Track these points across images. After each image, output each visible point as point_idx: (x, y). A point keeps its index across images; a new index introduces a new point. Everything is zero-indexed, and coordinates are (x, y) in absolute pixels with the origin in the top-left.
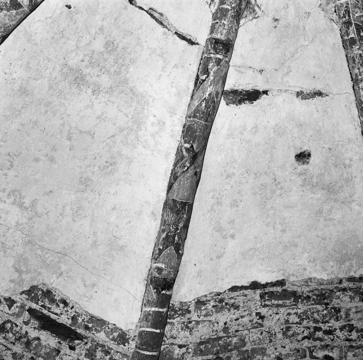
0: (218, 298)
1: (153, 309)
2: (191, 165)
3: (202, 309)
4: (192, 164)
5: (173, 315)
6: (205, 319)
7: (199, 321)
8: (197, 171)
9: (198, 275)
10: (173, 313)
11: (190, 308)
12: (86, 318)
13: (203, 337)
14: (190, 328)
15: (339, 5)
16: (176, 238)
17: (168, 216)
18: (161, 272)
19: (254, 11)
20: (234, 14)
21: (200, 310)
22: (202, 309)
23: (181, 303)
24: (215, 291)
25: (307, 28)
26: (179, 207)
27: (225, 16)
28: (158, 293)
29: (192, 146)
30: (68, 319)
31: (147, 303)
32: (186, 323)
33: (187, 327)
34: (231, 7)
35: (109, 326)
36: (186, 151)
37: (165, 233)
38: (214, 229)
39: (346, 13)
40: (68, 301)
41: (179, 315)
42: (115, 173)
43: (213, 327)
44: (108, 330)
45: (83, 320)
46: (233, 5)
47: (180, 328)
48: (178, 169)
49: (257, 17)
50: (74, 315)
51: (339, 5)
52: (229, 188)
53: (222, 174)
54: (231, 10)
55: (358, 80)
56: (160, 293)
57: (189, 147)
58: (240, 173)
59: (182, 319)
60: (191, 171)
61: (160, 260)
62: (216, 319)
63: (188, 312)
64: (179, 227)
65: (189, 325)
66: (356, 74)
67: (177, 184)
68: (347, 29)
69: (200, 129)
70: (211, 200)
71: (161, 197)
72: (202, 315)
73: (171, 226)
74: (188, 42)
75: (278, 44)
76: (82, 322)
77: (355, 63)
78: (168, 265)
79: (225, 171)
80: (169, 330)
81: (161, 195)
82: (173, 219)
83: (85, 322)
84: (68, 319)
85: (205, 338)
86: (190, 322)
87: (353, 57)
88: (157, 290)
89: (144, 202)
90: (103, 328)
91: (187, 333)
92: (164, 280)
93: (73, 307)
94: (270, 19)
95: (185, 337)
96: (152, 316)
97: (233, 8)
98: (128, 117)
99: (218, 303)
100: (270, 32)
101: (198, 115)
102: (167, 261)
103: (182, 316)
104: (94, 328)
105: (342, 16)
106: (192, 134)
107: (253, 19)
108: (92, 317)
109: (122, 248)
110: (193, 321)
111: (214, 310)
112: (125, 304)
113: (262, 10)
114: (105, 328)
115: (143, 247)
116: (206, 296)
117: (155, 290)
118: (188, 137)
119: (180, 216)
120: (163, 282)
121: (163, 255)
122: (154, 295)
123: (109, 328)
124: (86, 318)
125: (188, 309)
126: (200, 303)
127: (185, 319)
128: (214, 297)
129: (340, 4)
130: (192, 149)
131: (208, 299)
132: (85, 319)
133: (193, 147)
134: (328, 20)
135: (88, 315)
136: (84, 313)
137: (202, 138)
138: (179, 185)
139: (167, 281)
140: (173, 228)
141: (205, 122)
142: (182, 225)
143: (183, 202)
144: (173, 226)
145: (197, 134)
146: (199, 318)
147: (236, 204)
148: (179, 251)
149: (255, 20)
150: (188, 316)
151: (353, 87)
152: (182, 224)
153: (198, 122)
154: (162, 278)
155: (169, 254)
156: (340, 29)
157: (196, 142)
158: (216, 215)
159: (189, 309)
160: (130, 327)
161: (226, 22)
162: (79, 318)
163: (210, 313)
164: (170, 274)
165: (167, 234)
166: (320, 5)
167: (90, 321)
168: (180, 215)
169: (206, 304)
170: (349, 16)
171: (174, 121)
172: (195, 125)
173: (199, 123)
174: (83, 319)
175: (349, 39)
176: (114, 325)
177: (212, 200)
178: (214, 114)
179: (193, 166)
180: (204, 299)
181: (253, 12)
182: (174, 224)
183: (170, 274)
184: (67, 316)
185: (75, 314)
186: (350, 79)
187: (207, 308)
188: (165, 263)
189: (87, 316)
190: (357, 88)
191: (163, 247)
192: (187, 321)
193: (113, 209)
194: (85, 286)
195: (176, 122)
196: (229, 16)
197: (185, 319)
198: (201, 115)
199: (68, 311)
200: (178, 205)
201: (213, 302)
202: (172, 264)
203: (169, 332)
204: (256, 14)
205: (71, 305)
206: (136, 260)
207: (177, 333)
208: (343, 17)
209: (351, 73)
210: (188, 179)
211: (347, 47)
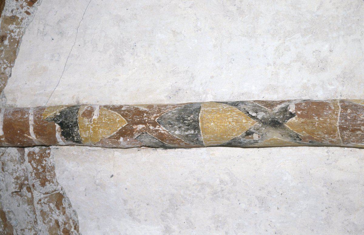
0: (71, 227)
1: (31, 118)
2: (261, 121)
3: (51, 204)
4: (263, 123)
5: (34, 159)
6: (38, 213)
7: (33, 204)
8: (254, 135)
9: (97, 185)
10: (38, 158)
11: (49, 183)
12: (16, 34)
13: (11, 216)
14: (20, 191)
16: (140, 127)
17: (173, 108)
18: (86, 116)
21: (49, 202)
22: (51, 204)
23: (53, 168)
24: (80, 218)
26: (189, 118)
28: (56, 119)
29: (292, 115)
30: (12, 11)
31: (40, 110)
32: (26, 182)
33: (21, 186)
35: (8, 69)
36: (282, 108)
37: (146, 109)
38: (173, 195)
40: (35, 4)
41: (36, 169)
42: (228, 18)
43: (29, 229)
44: (2, 68)
45: (13, 30)
47: (17, 174)
48: (250, 104)
50: (18, 18)
52: (243, 206)
53: (263, 188)
56: (56, 121)
57: (290, 110)
58: (273, 221)
59: (31, 175)
60: (250, 124)
61: (105, 110)
62: (40, 231)
63: (43, 181)
64: (158, 126)
65: (25, 189)
67: (225, 107)
69: (325, 122)
70: (218, 180)
71: (204, 95)
72: (42, 207)
73: (158, 115)
76: (9, 30)
78: (97, 123)
79: (269, 192)
80: (12, 157)
81: (208, 96)
82: (169, 114)
83: (9, 34)
84: (12, 11)
85: (10, 219)
86: (29, 189)
88: (59, 116)
89: (192, 74)
90: (5, 60)
91: (13, 188)
92: (75, 123)
93: (28, 13)
95: (6, 185)
96: (21, 118)
98: (318, 9)
99: (63, 228)
101: (349, 111)
102: (104, 121)
103: (35, 174)
104: (3, 48)
106: (313, 110)
108: (18, 42)
109: (119, 60)
110: (32, 193)
111: (51, 224)
112: (40, 83)
114: (4, 63)
115: (126, 90)
116: (70, 206)
117: (59, 114)
118: (307, 106)
119: (175, 125)
120: (72, 121)
121: (112, 113)
122: (51, 114)
123: (5, 68)
124: (16, 34)
125: (47, 181)
126: (59, 199)
127: (33, 180)
128: (71, 221)
130: (288, 115)
131: (68, 211)
132: (14, 33)
133: (291, 117)
135: (20, 36)
136: (22, 30)
137: (310, 128)
138: (225, 111)
139: (74, 128)
140: (156, 117)
141: (341, 127)
142: (162, 132)
143: (198, 122)
144: (158, 116)
145: (316, 118)
146: (38, 203)
147: (219, 224)
148: (123, 137)
150: (38, 183)
152: (164, 130)
153: (337, 114)
154: (77, 119)
155: (114, 120)
157: (303, 120)
158: (194, 195)
159: (47, 183)
160: (9, 97)
162: (14, 25)
163: (47, 220)
164: (85, 131)
165: (145, 112)
167: (12, 41)
168: (176, 123)
169: (58, 209)
171: (331, 84)
172: (330, 112)
173: (335, 117)
174: (14, 31)
176: (10, 75)
177: (218, 181)
178: (357, 141)
179: (260, 125)
180: (65, 205)
182: (161, 117)
183: (85, 131)
184: (15, 8)
185: (20, 18)
187: (53, 212)
188: (100, 119)
189: (18, 35)
191: (124, 111)
192: (31, 183)
193: (174, 32)
194: (60, 21)
195: (331, 88)
197: (33, 180)
198: (350, 116)
199: (22, 8)
200: (192, 116)
201: (63, 220)
202: (101, 131)
203: (9, 158)
205: (31, 10)
206: (105, 85)
207: (10, 171)
210: (237, 121)
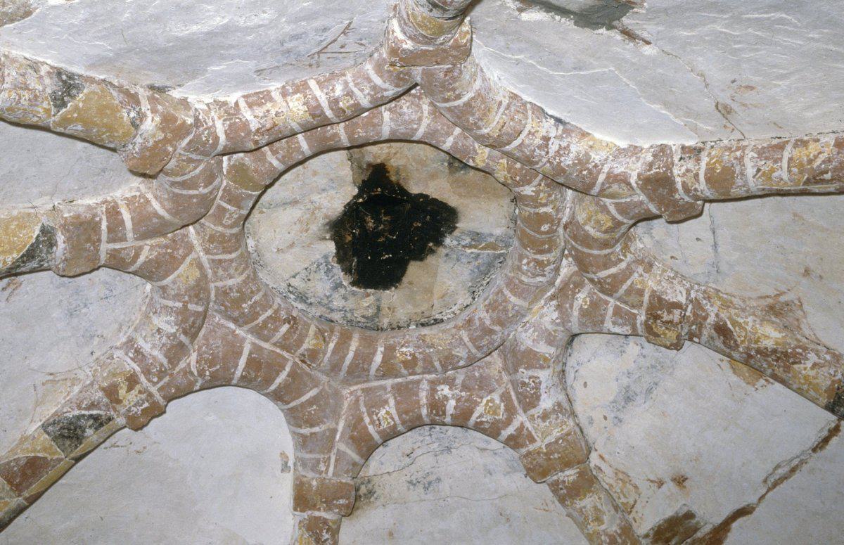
19: (788, 305)
20: (782, 367)
74: (834, 435)
107: (802, 310)
113: (786, 291)
149: (805, 307)
181: (789, 307)
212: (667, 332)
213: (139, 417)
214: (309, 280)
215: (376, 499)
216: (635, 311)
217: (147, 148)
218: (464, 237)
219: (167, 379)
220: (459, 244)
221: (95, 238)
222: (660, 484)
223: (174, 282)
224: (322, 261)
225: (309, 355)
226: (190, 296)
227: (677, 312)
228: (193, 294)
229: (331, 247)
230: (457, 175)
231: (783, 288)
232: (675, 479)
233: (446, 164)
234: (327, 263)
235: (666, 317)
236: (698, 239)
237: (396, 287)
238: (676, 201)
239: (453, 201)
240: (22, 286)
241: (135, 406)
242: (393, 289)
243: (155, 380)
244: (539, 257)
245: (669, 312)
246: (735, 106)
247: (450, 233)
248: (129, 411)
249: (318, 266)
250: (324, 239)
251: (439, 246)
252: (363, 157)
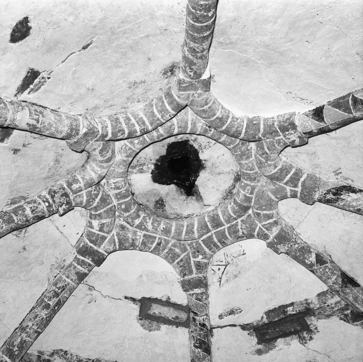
15: (63, 279)
19: (20, 231)
25: (33, 270)
27: (9, 223)
34: (17, 222)
39: (62, 288)
46: (19, 222)
49: (18, 237)
51: (63, 279)
54: (15, 224)
55: (25, 330)
66: (27, 326)
68: (52, 297)
75: (9, 263)
77: (34, 319)
87: (38, 315)
94: (23, 245)
97: (18, 224)
100: (14, 252)
105: (58, 286)
129: (65, 280)
134: (46, 278)
151: (16, 329)
156: (47, 289)
161: (4, 228)
166: (53, 265)
170: (62, 292)
175: (47, 303)
186: (20, 322)
190: (19, 334)
196: (10, 225)
204: (20, 234)
208: (57, 288)
209: (24, 319)
211: (41, 305)
212: (60, 200)
213: (291, 128)
214: (208, 142)
215: (161, 72)
216: (75, 195)
217: (283, 243)
218: (147, 169)
219: (276, 138)
220: (147, 165)
221: (302, 195)
222: (24, 146)
223: (271, 171)
224: (204, 150)
225: (208, 131)
226: (265, 165)
227: (62, 212)
228: (263, 165)
229: (202, 156)
230: (159, 198)
231: (26, 234)
232: (19, 150)
233: (164, 201)
234: (201, 149)
235: (64, 206)
236: (65, 226)
237: (169, 144)
238: (89, 256)
239: (157, 186)
240: (333, 171)
241: (292, 134)
242: (170, 143)
243: (281, 141)
244: (119, 191)
245: (64, 209)
246: (89, 292)
247: (153, 171)
248: (295, 132)
249: (205, 148)
250: (205, 160)
251: (155, 163)
252: (196, 198)
